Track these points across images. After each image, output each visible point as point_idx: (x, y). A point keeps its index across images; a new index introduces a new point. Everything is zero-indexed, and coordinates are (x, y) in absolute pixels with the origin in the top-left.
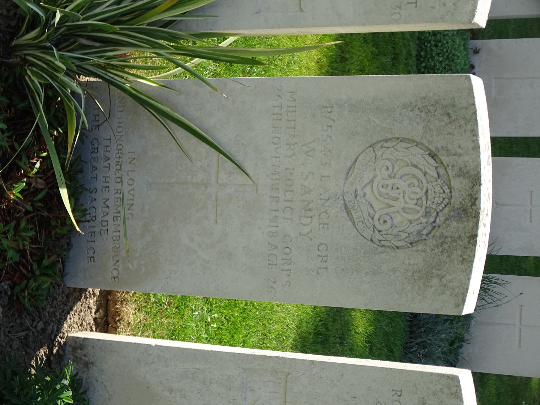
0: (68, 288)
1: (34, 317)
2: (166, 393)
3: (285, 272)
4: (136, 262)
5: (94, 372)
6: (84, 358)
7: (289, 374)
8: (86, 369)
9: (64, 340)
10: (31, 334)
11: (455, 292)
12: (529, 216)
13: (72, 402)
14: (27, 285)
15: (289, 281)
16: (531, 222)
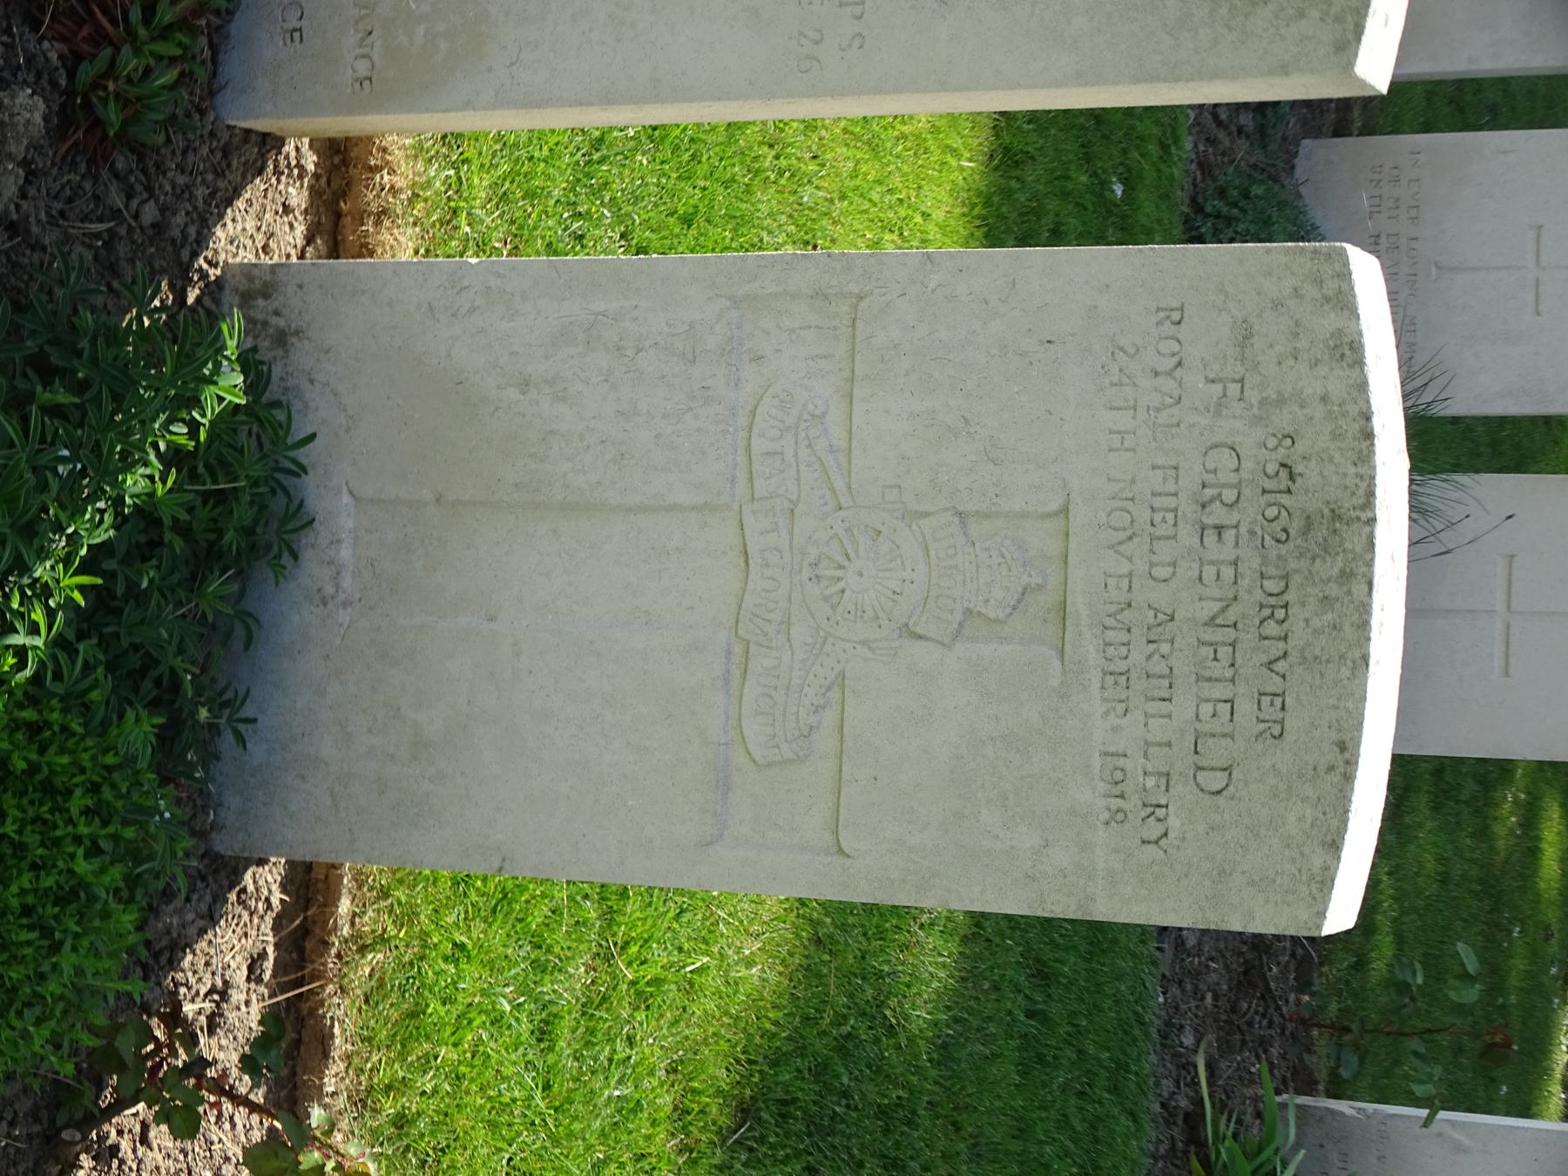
0: (229, 127)
1: (132, 187)
2: (513, 394)
3: (849, 9)
4: (421, 30)
5: (302, 356)
6: (274, 320)
7: (861, 298)
8: (280, 352)
9: (218, 272)
10: (123, 231)
11: (1333, 10)
13: (244, 402)
14: (112, 63)
15: (859, 35)
16: (1538, 313)
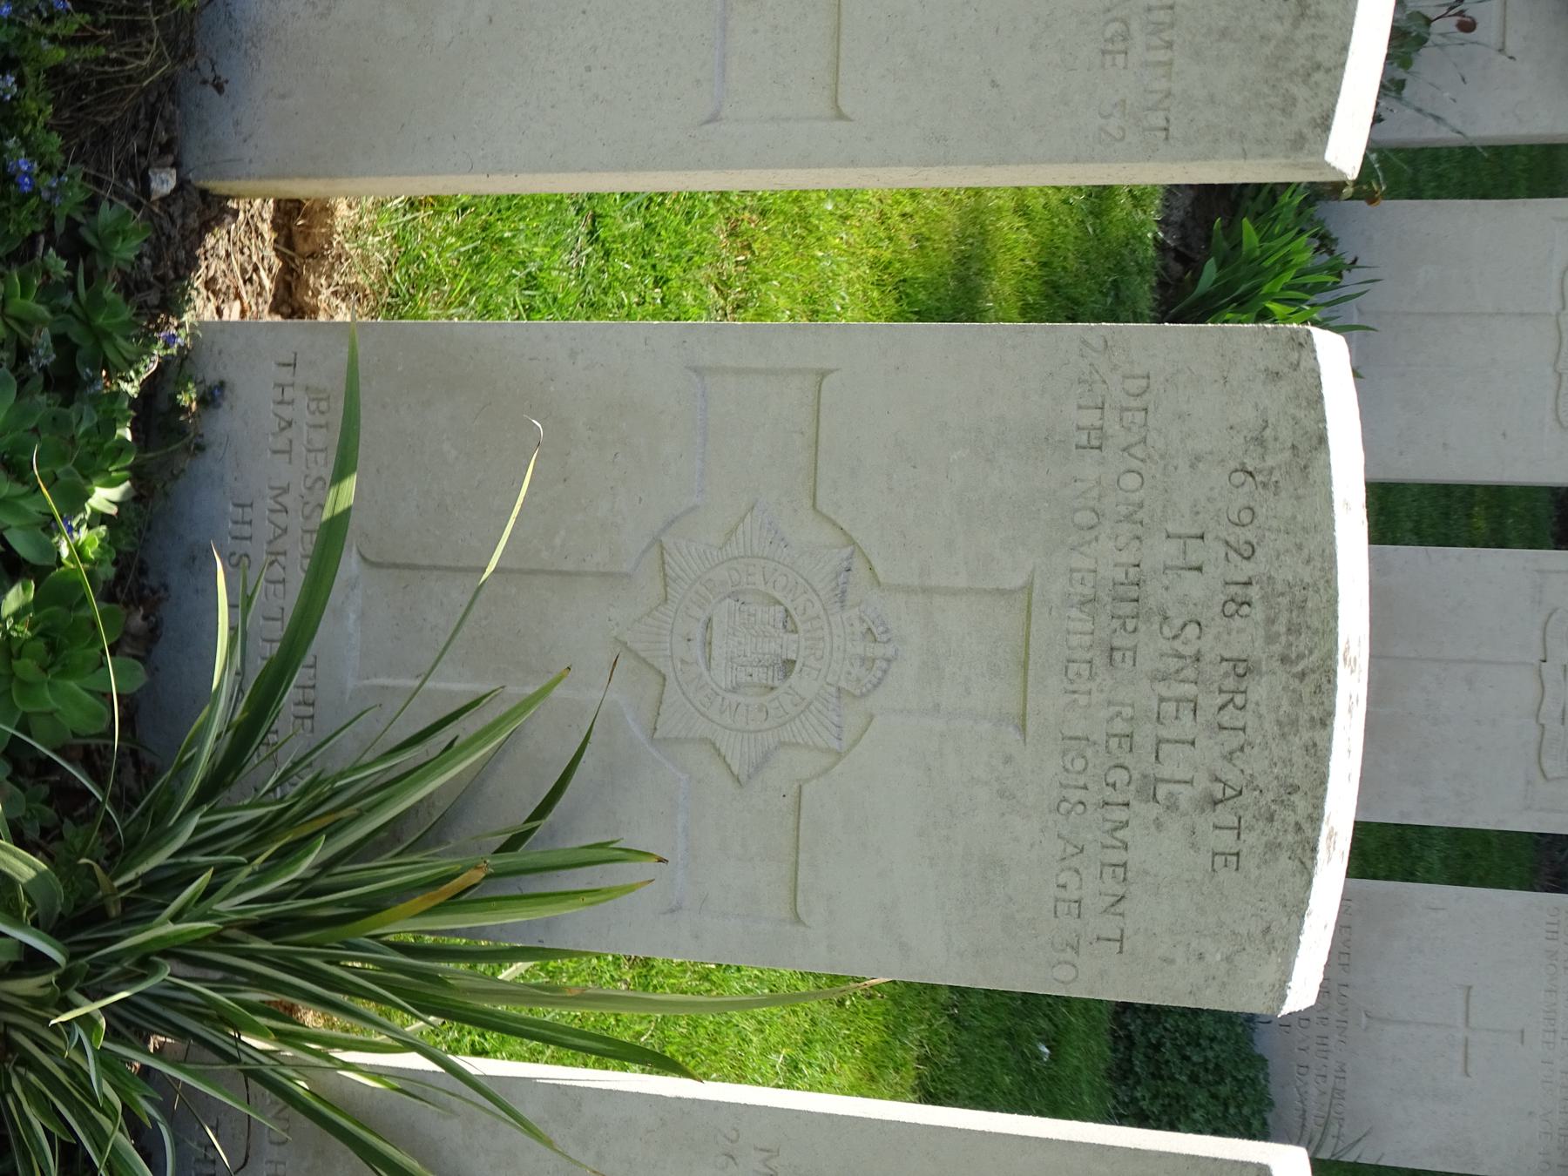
12: (1459, 1057)
